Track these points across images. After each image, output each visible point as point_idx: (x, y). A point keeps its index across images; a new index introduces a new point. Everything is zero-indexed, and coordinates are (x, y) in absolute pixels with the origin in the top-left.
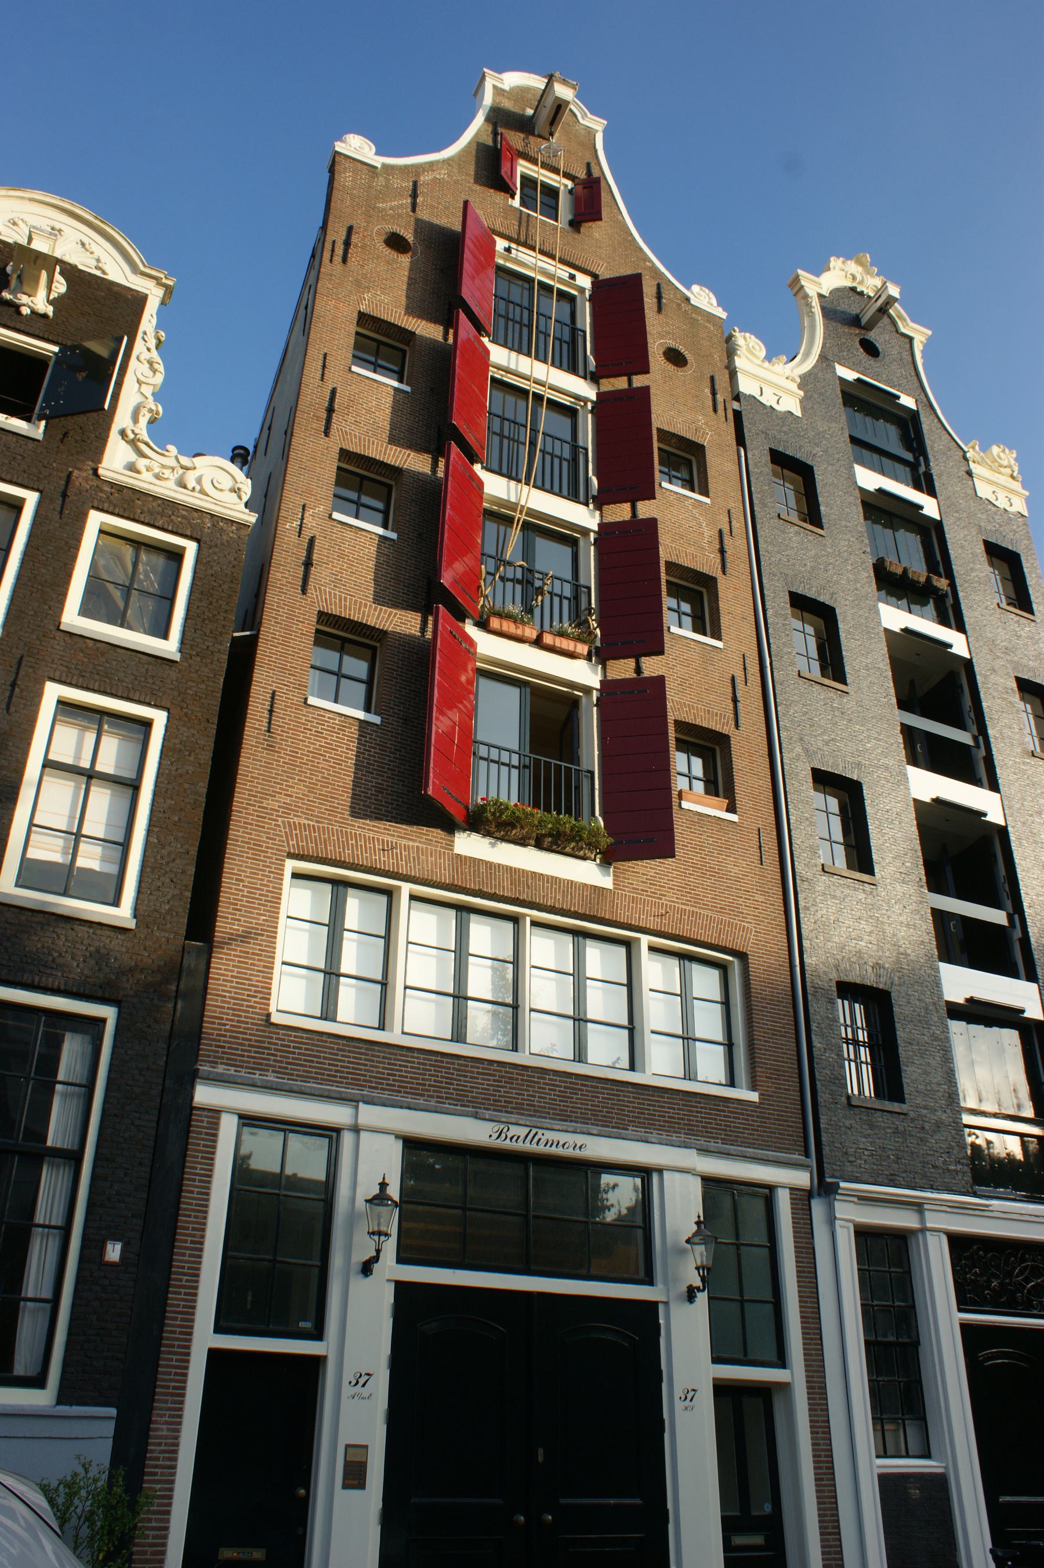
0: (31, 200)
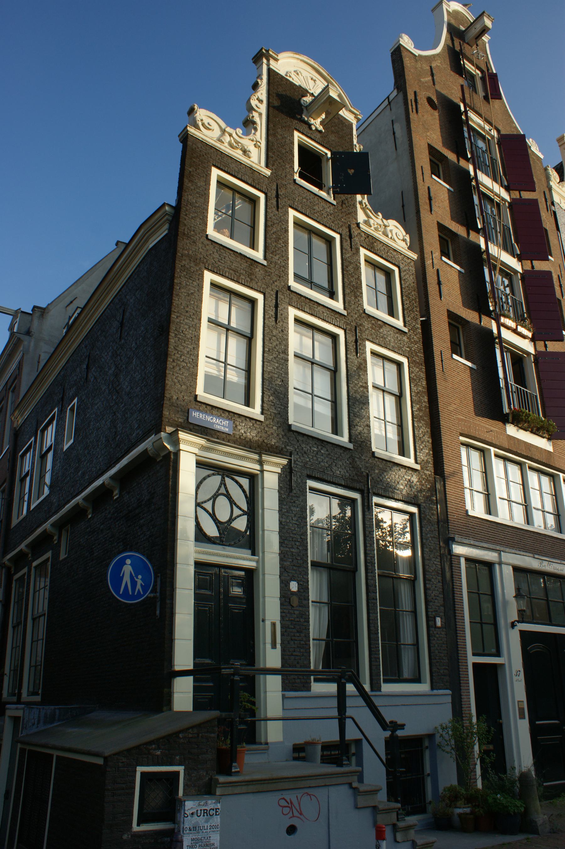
0: (302, 60)
